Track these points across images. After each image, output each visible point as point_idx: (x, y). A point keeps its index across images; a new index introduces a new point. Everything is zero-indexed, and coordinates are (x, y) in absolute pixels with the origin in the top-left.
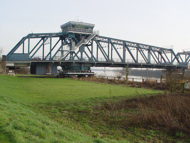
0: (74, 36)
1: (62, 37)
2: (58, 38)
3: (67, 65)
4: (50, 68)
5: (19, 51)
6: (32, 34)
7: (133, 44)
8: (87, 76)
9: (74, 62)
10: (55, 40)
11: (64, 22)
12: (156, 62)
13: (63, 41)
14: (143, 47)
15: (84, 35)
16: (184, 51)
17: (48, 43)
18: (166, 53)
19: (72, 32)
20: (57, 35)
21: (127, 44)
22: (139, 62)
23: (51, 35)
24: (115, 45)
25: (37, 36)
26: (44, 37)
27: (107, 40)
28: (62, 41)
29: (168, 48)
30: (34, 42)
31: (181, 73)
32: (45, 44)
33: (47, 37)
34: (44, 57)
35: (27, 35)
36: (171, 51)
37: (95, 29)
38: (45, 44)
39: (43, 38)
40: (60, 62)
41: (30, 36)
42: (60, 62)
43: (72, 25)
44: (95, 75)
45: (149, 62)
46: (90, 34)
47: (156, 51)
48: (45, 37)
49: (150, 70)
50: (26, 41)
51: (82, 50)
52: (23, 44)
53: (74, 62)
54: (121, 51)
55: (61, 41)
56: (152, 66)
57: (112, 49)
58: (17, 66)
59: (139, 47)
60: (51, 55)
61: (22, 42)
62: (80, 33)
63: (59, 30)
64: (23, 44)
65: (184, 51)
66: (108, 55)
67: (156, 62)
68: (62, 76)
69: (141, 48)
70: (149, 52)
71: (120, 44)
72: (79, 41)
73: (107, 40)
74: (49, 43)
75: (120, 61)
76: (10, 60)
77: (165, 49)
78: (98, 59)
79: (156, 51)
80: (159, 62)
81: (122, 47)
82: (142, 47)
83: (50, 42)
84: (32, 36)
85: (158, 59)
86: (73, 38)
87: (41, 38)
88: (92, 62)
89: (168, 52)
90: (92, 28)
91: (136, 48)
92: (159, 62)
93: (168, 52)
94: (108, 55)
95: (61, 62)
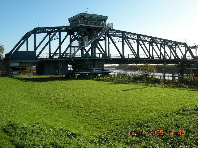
0: (85, 30)
1: (70, 31)
2: (66, 33)
3: (78, 63)
4: (60, 67)
5: (23, 48)
6: (39, 28)
7: (133, 36)
8: (99, 75)
9: (88, 59)
10: (64, 34)
11: (74, 13)
12: (147, 55)
13: (72, 36)
14: (157, 41)
15: (95, 28)
16: (196, 45)
17: (56, 38)
18: (181, 47)
19: (84, 25)
20: (66, 29)
21: (127, 35)
22: (126, 56)
23: (59, 30)
24: (112, 37)
25: (43, 30)
26: (51, 31)
27: (120, 33)
28: (70, 37)
29: (182, 42)
30: (40, 37)
31: (196, 68)
32: (55, 39)
33: (55, 32)
34: (51, 55)
35: (32, 29)
36: (185, 44)
37: (108, 22)
38: (55, 39)
39: (49, 33)
40: (72, 60)
41: (36, 31)
42: (72, 60)
43: (83, 17)
44: (110, 73)
45: (152, 57)
46: (103, 27)
47: (158, 43)
48: (52, 32)
49: (134, 65)
50: (31, 38)
51: (94, 46)
52: (26, 41)
53: (88, 59)
54: (120, 45)
55: (69, 36)
56: (142, 61)
57: (109, 43)
58: (23, 66)
59: (126, 37)
60: (162, 55)
61: (25, 38)
62: (93, 26)
63: (67, 24)
64: (26, 41)
65: (196, 45)
66: (59, 49)
67: (147, 55)
68: (70, 76)
69: (128, 38)
70: (138, 44)
71: (117, 36)
72: (91, 35)
73: (120, 33)
74: (57, 38)
75: (119, 56)
76: (15, 60)
77: (179, 43)
78: (125, 55)
79: (158, 43)
80: (150, 55)
81: (121, 39)
82: (129, 36)
83: (58, 37)
84: (38, 30)
85: (149, 52)
86: (84, 32)
87: (46, 34)
88: (107, 59)
89: (181, 46)
90: (105, 20)
91: (136, 41)
92: (150, 55)
93: (181, 46)
94: (104, 50)
95: (74, 60)
